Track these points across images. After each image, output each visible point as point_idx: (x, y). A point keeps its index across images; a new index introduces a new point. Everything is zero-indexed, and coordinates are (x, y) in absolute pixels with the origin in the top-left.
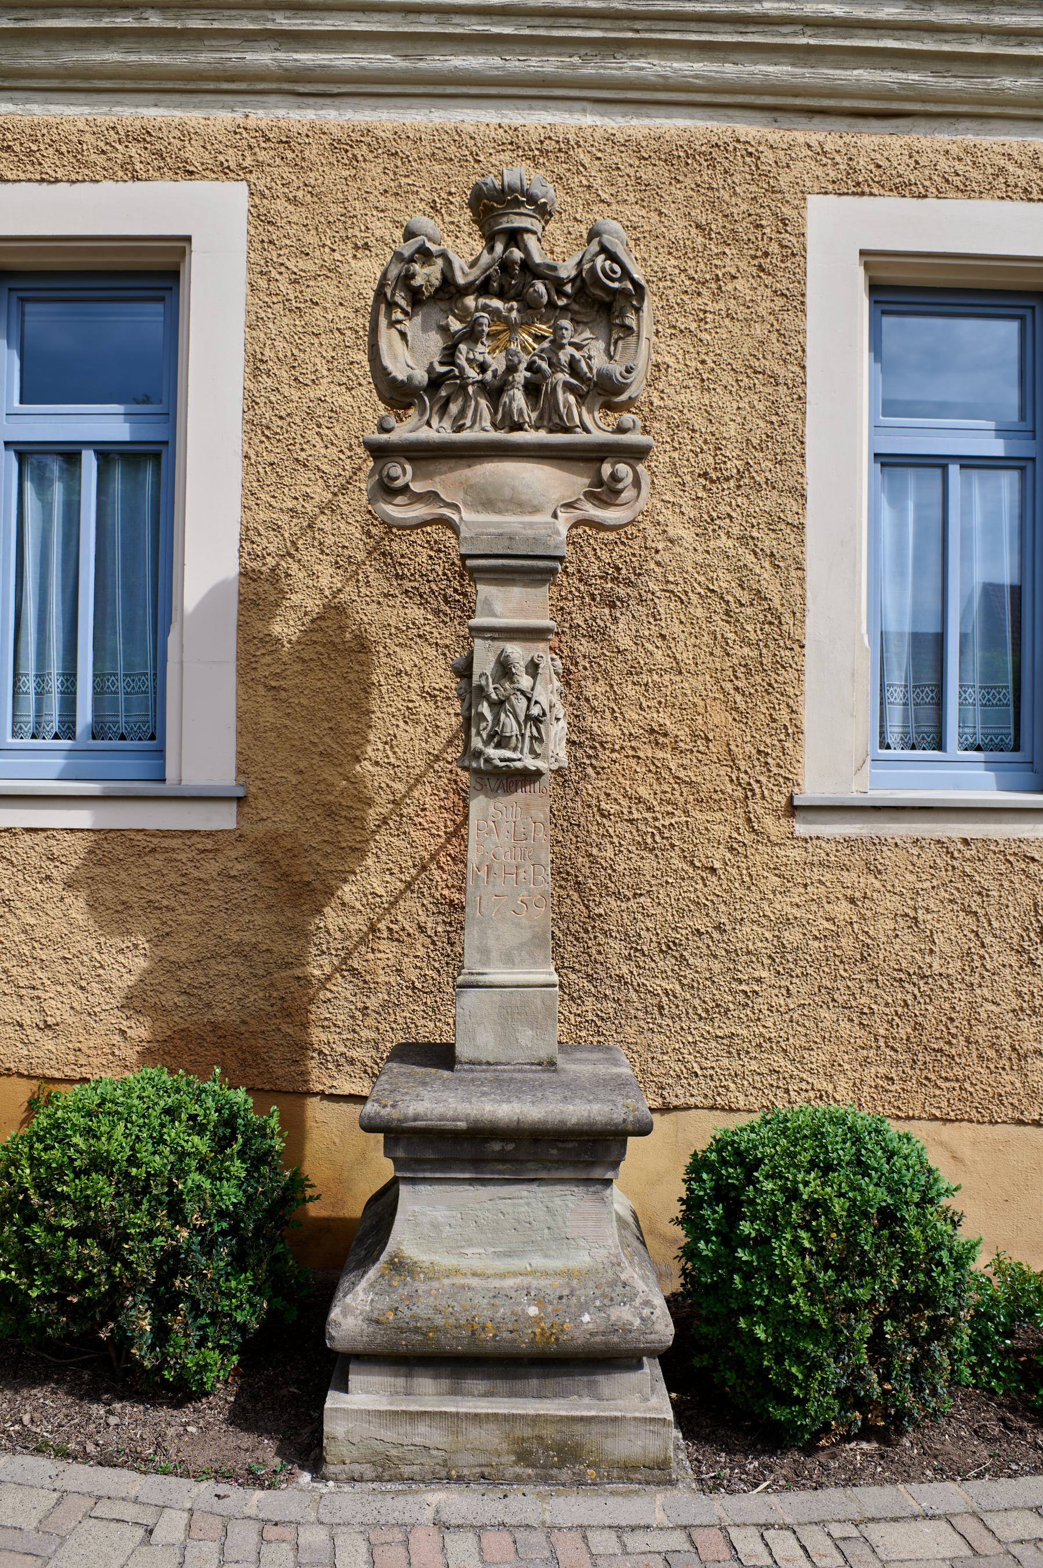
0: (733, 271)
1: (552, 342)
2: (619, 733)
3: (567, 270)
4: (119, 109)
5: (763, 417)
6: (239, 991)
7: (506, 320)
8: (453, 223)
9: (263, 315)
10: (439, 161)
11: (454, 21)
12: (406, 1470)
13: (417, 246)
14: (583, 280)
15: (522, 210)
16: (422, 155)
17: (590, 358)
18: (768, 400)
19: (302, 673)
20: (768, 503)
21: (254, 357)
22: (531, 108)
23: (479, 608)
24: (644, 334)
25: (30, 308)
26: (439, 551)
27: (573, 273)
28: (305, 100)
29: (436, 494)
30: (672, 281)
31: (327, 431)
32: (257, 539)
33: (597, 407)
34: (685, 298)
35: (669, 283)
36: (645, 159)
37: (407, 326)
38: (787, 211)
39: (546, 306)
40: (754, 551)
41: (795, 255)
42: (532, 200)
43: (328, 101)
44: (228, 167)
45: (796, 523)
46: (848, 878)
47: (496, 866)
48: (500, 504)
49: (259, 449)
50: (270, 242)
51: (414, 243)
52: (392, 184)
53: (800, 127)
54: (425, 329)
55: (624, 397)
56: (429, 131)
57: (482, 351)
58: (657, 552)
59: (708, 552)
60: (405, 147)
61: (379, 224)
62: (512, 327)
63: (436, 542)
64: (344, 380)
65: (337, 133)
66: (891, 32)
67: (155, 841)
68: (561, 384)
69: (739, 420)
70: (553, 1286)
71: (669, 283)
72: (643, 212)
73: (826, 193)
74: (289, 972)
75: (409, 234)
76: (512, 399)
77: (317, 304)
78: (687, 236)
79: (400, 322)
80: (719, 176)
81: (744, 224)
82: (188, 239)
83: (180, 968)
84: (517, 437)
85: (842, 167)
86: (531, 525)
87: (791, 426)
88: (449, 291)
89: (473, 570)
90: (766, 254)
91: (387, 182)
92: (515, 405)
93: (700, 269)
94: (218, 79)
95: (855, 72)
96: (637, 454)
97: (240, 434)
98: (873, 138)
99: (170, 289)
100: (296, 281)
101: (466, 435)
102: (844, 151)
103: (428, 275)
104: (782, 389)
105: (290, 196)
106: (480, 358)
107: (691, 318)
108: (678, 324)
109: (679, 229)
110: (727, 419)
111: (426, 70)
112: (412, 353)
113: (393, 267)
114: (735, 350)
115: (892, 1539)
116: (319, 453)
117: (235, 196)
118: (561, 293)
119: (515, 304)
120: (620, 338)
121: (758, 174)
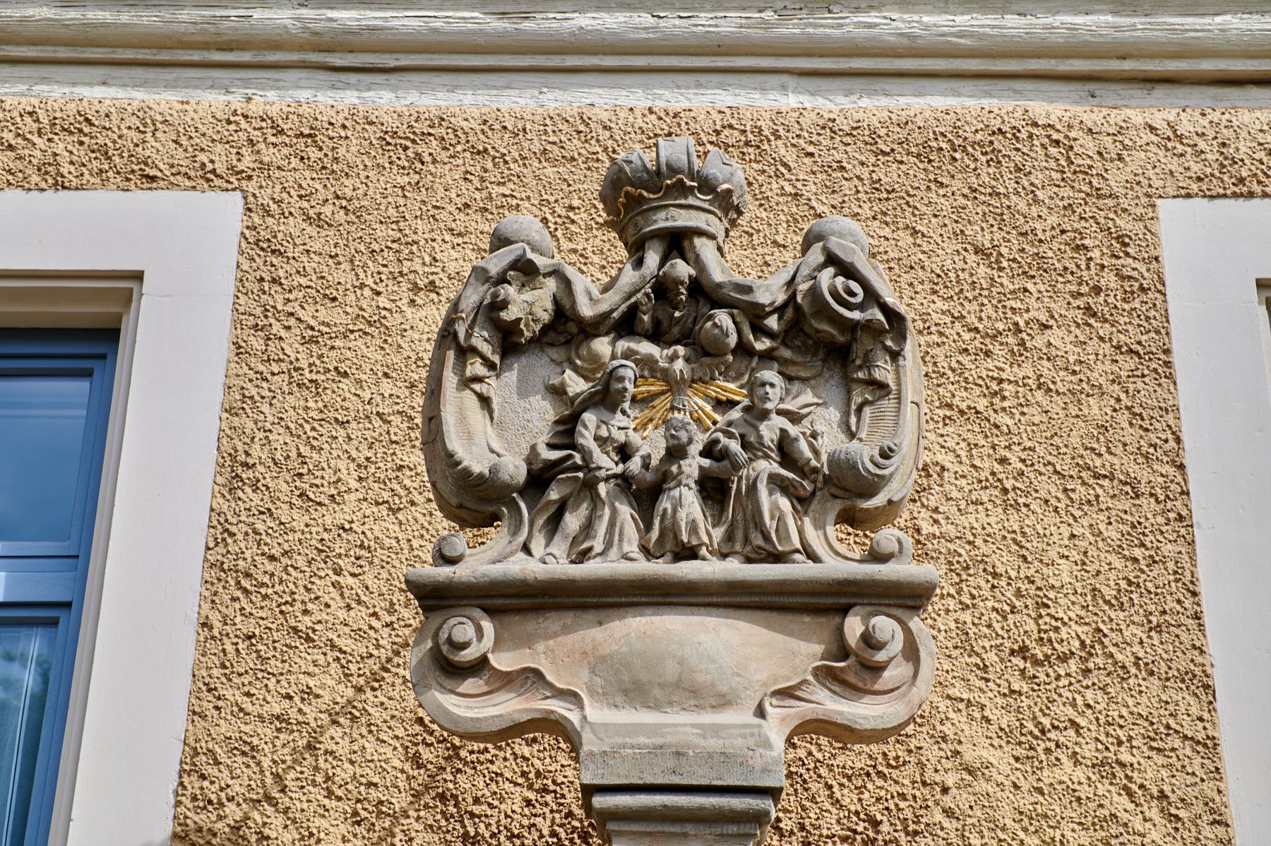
0: (1043, 317)
1: (747, 410)
3: (770, 292)
4: (44, 87)
5: (1118, 550)
7: (666, 375)
8: (575, 251)
9: (254, 392)
10: (554, 162)
13: (512, 257)
14: (798, 308)
15: (691, 201)
16: (526, 153)
17: (814, 435)
18: (1123, 522)
20: (1144, 700)
21: (233, 458)
22: (699, 85)
24: (909, 395)
26: (545, 790)
27: (781, 298)
28: (344, 77)
29: (538, 674)
30: (941, 334)
31: (351, 581)
32: (211, 770)
33: (831, 517)
34: (965, 359)
35: (935, 338)
36: (884, 153)
37: (492, 387)
38: (1125, 224)
39: (734, 352)
40: (1125, 788)
41: (1147, 289)
42: (707, 185)
43: (379, 78)
44: (213, 171)
45: (1200, 736)
48: (657, 692)
49: (230, 612)
50: (274, 281)
51: (506, 255)
52: (477, 195)
53: (1133, 103)
54: (523, 392)
56: (537, 118)
57: (622, 425)
58: (945, 790)
59: (1040, 791)
60: (499, 142)
61: (454, 254)
62: (674, 385)
63: (538, 774)
64: (386, 495)
65: (391, 122)
69: (1075, 556)
71: (935, 338)
72: (887, 231)
73: (1188, 196)
75: (500, 241)
76: (677, 504)
77: (345, 375)
78: (960, 265)
79: (478, 379)
80: (1007, 176)
81: (1055, 246)
82: (138, 276)
84: (688, 570)
85: (1209, 156)
86: (716, 729)
87: (1171, 566)
88: (566, 330)
90: (1097, 290)
91: (469, 192)
92: (682, 514)
93: (990, 316)
94: (206, 46)
95: (1218, 19)
96: (909, 598)
97: (197, 586)
98: (1258, 114)
99: (104, 357)
100: (314, 340)
101: (594, 568)
102: (1211, 133)
103: (531, 304)
104: (1147, 503)
105: (312, 213)
106: (620, 437)
107: (977, 391)
108: (956, 401)
109: (946, 255)
110: (1053, 554)
111: (534, 33)
112: (500, 429)
113: (470, 290)
114: (1057, 440)
116: (334, 616)
117: (224, 211)
118: (759, 330)
119: (681, 350)
120: (865, 403)
121: (1071, 170)
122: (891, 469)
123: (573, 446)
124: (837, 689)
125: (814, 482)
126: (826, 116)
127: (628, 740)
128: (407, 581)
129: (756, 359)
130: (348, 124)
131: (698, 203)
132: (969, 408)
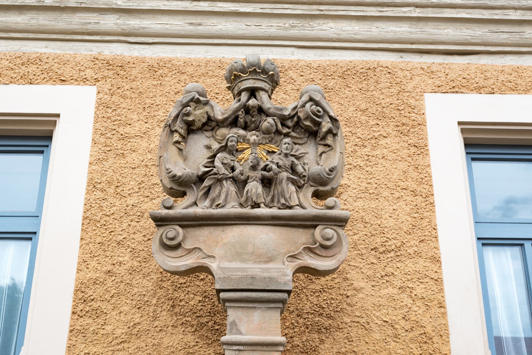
5: (409, 214)
11: (219, 5)
34: (356, 148)
39: (274, 133)
55: (328, 188)
66: (464, 10)
68: (285, 178)
82: (58, 116)
84: (257, 211)
86: (267, 270)
89: (226, 300)
95: (446, 31)
96: (340, 222)
99: (47, 146)
108: (353, 163)
120: (324, 152)
122: (333, 176)
124: (312, 255)
125: (304, 181)
126: (308, 62)
127: (234, 274)
128: (150, 215)
129: (282, 136)
130: (135, 62)
131: (261, 78)
132: (358, 165)
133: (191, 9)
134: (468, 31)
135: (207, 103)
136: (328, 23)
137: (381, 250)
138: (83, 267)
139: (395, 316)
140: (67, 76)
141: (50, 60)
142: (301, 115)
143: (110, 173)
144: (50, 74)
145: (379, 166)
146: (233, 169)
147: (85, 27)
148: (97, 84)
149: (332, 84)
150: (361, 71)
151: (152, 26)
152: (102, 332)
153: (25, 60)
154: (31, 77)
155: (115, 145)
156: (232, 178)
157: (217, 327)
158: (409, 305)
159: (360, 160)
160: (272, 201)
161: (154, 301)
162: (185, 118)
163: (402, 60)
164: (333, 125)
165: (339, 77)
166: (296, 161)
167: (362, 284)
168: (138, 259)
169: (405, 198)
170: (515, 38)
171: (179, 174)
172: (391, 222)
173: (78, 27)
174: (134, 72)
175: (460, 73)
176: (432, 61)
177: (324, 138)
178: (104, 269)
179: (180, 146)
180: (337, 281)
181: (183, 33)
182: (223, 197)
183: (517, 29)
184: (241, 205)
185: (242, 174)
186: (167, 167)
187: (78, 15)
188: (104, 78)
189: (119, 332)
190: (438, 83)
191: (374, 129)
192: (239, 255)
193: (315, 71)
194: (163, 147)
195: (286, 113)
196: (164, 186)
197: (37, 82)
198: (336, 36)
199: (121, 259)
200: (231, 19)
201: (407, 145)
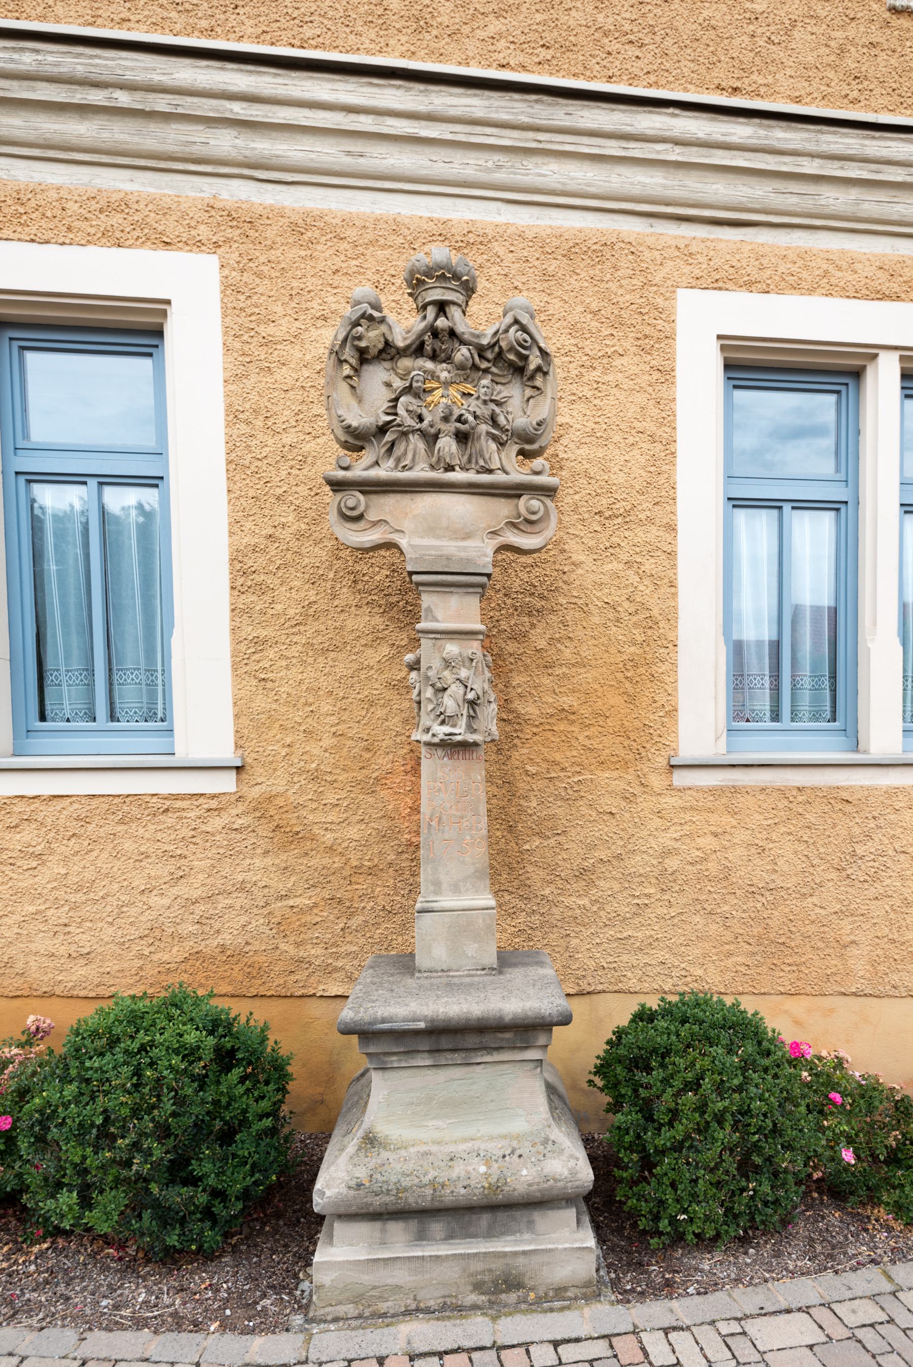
2: (538, 712)
5: (644, 468)
6: (243, 919)
12: (383, 1307)
19: (287, 668)
23: (423, 614)
25: (30, 356)
34: (583, 370)
46: (714, 818)
47: (444, 817)
55: (535, 446)
60: (351, 233)
67: (168, 803)
70: (496, 1148)
74: (285, 903)
82: (168, 302)
83: (193, 903)
86: (465, 549)
89: (418, 584)
95: (714, 187)
96: (549, 491)
99: (157, 346)
115: (768, 1333)
123: (396, 414)
133: (347, 128)
134: (745, 189)
135: (383, 320)
136: (549, 163)
137: (607, 514)
138: (236, 529)
139: (618, 596)
140: (170, 237)
141: (142, 206)
142: (503, 344)
143: (254, 396)
144: (146, 231)
145: (611, 398)
146: (421, 419)
147: (187, 149)
148: (219, 251)
149: (552, 267)
150: (594, 247)
151: (289, 153)
152: (271, 612)
153: (103, 203)
154: (118, 234)
155: (256, 353)
156: (419, 430)
157: (410, 608)
158: (636, 584)
159: (586, 388)
160: (469, 461)
161: (331, 575)
162: (356, 343)
163: (652, 230)
164: (543, 359)
165: (564, 256)
166: (497, 410)
167: (582, 558)
168: (306, 520)
169: (641, 445)
170: (807, 204)
171: (355, 424)
172: (621, 478)
173: (176, 149)
174: (270, 233)
175: (728, 257)
176: (693, 234)
177: (532, 378)
178: (264, 532)
179: (352, 383)
180: (552, 553)
181: (337, 168)
182: (410, 456)
183: (811, 188)
184: (432, 467)
185: (432, 426)
186: (340, 413)
187: (174, 126)
188: (227, 241)
189: (291, 612)
190: (697, 273)
191: (608, 342)
192: (432, 528)
193: (531, 244)
194: (331, 383)
195: (485, 342)
196: (338, 440)
197: (128, 243)
198: (559, 187)
199: (283, 520)
200: (408, 148)
201: (648, 368)
